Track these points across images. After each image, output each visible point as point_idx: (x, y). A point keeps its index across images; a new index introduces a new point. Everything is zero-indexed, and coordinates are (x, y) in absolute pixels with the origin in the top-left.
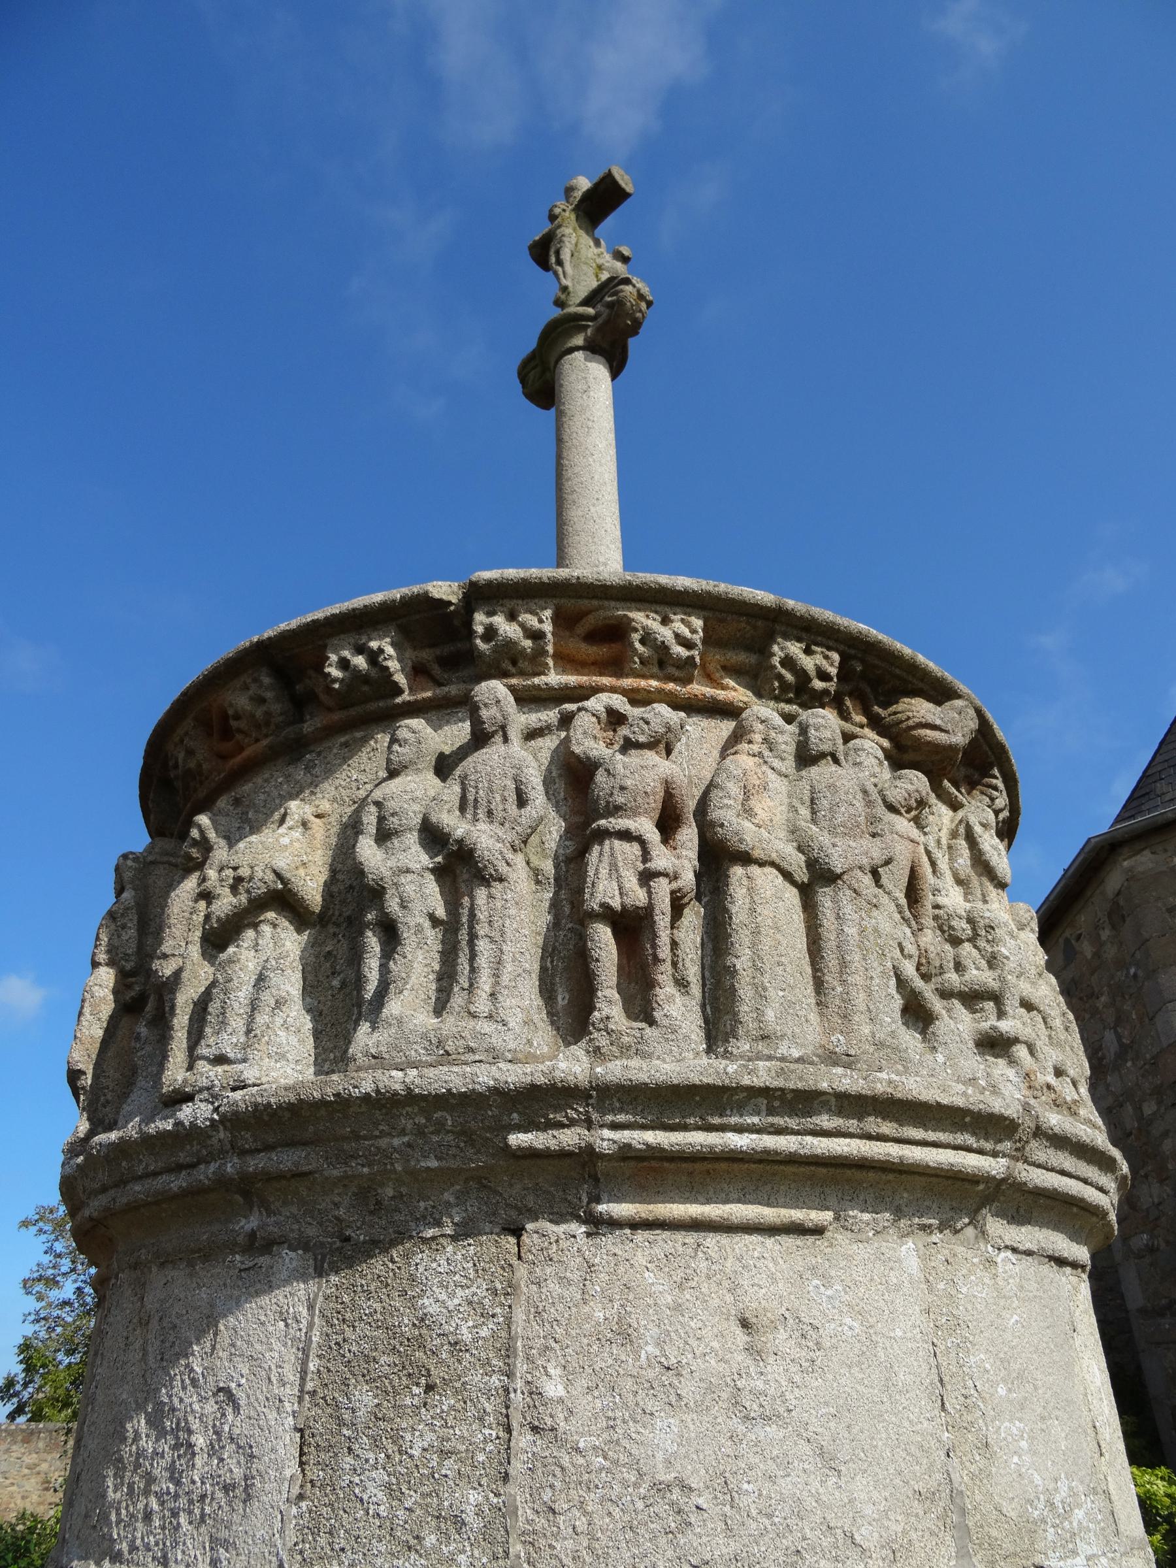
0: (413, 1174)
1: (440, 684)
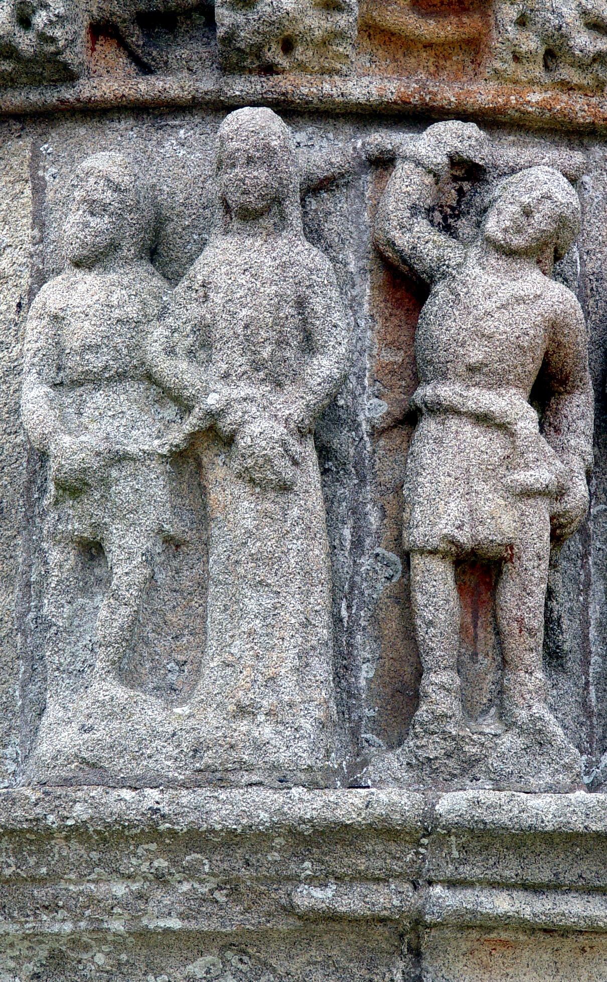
0: (144, 935)
1: (146, 69)
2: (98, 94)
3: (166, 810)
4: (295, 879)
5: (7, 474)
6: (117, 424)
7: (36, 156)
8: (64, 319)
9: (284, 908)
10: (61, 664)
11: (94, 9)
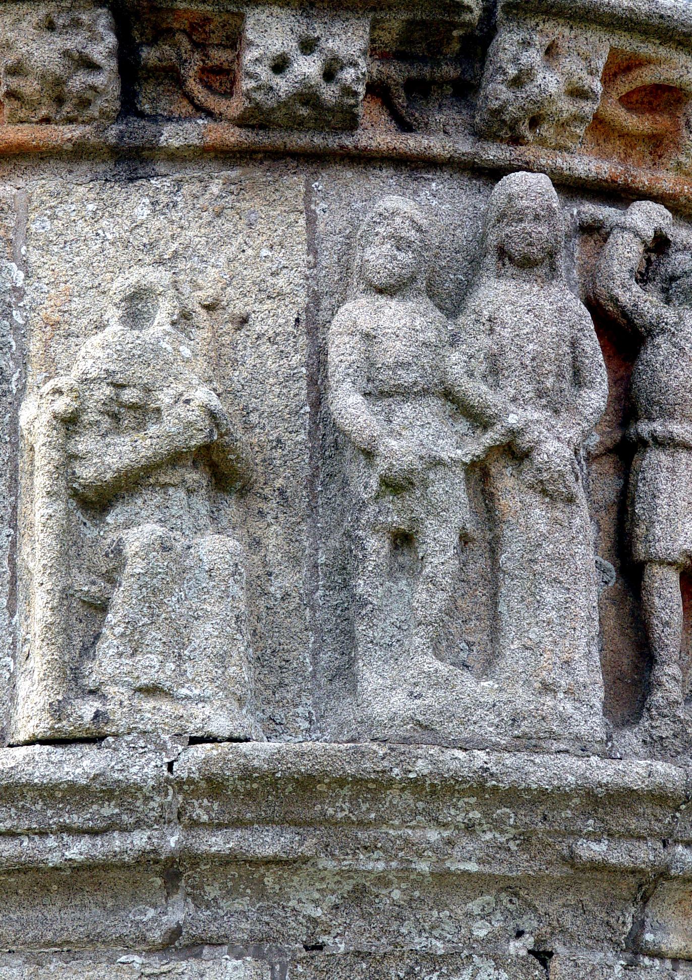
1: (405, 127)
2: (374, 144)
3: (494, 770)
4: (578, 834)
5: (290, 468)
6: (426, 433)
7: (309, 191)
8: (375, 337)
9: (563, 858)
10: (375, 638)
11: (374, 71)
